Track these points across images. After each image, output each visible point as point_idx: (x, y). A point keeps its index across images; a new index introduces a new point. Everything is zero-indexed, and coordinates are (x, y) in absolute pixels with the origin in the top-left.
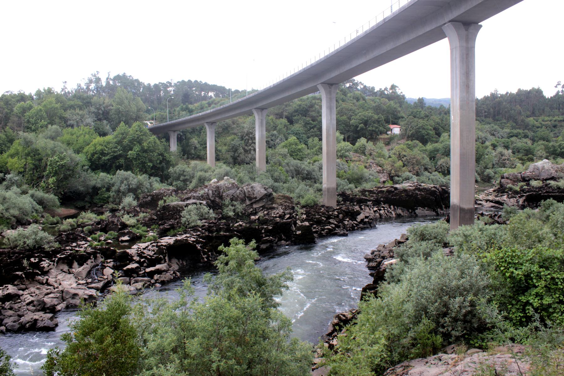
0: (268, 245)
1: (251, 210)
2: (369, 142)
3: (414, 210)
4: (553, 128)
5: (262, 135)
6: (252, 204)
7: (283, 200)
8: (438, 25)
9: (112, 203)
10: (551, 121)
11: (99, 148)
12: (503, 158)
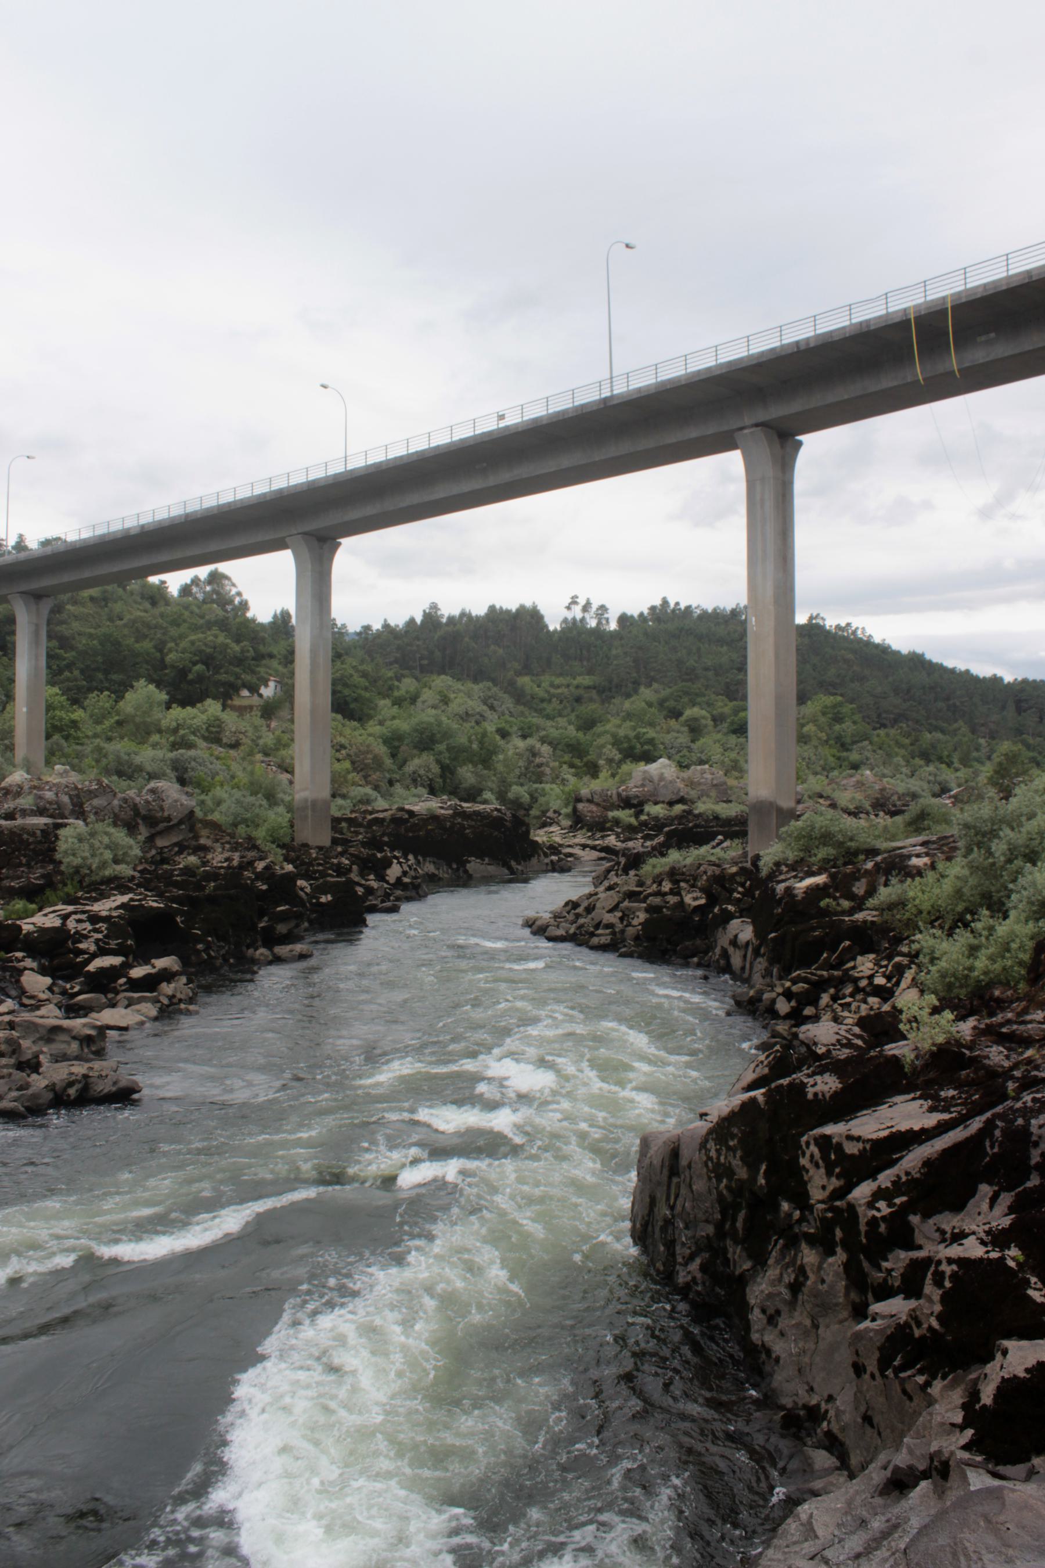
3: (463, 864)
4: (575, 704)
8: (726, 428)
10: (568, 686)
12: (538, 760)
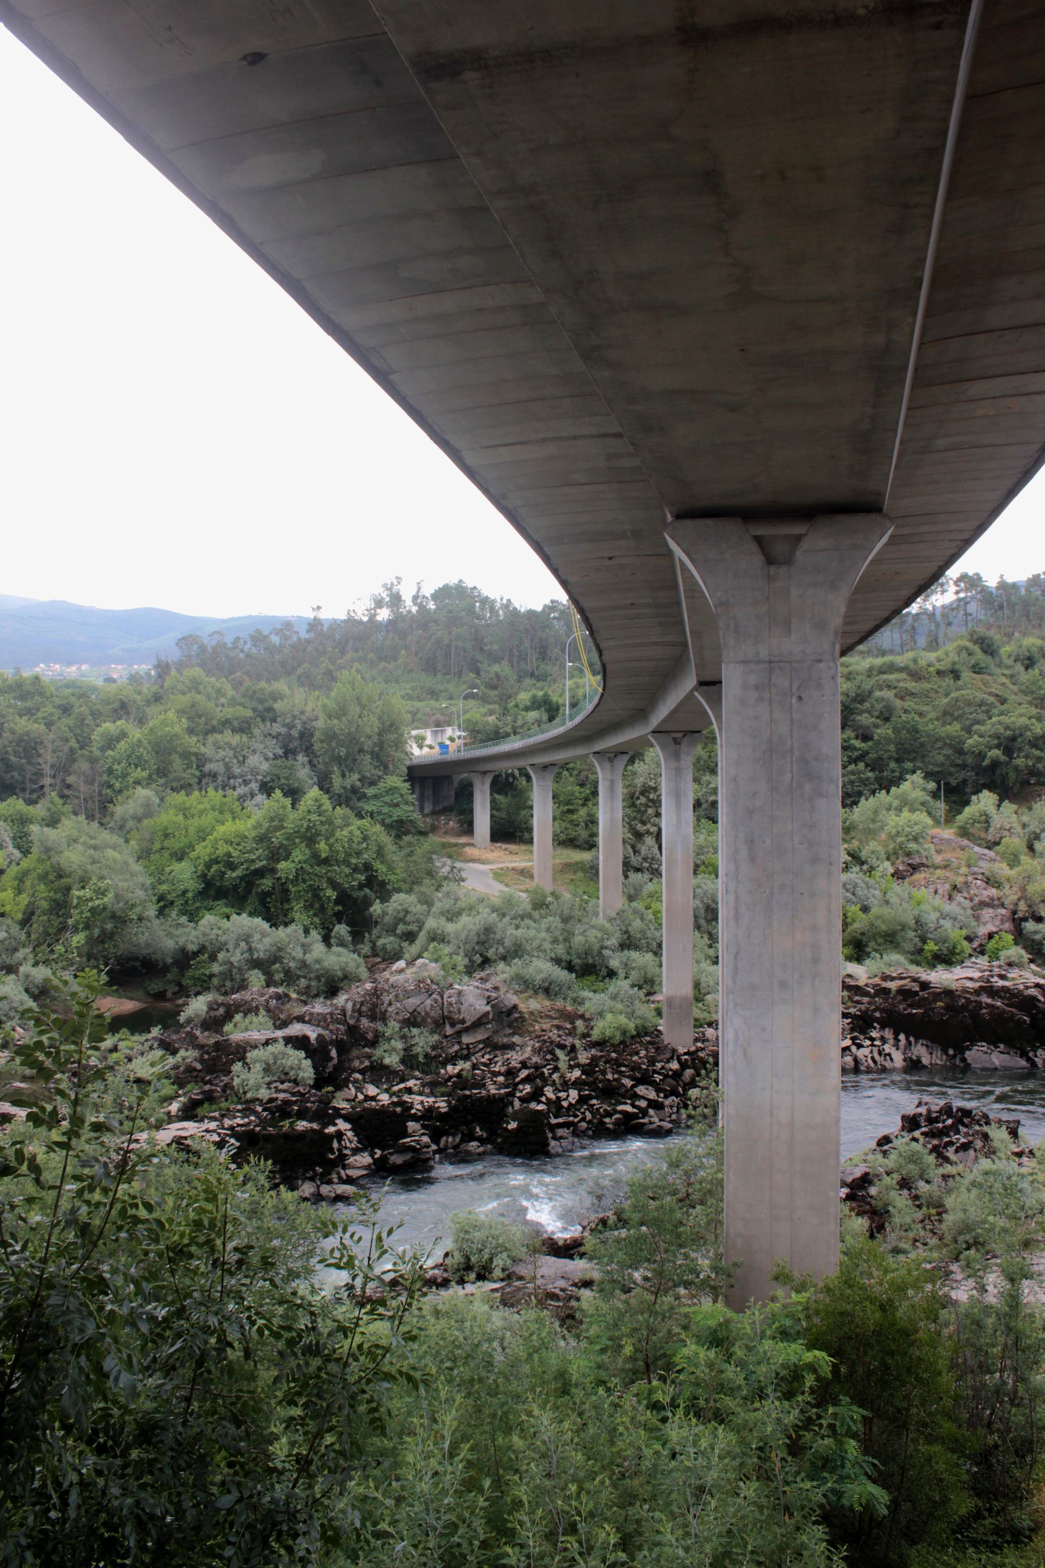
0: (408, 1156)
1: (456, 1047)
2: (1006, 803)
3: (961, 1050)
5: (612, 819)
6: (459, 1033)
7: (556, 1022)
9: (218, 990)
11: (223, 849)
